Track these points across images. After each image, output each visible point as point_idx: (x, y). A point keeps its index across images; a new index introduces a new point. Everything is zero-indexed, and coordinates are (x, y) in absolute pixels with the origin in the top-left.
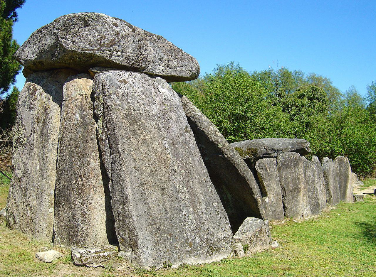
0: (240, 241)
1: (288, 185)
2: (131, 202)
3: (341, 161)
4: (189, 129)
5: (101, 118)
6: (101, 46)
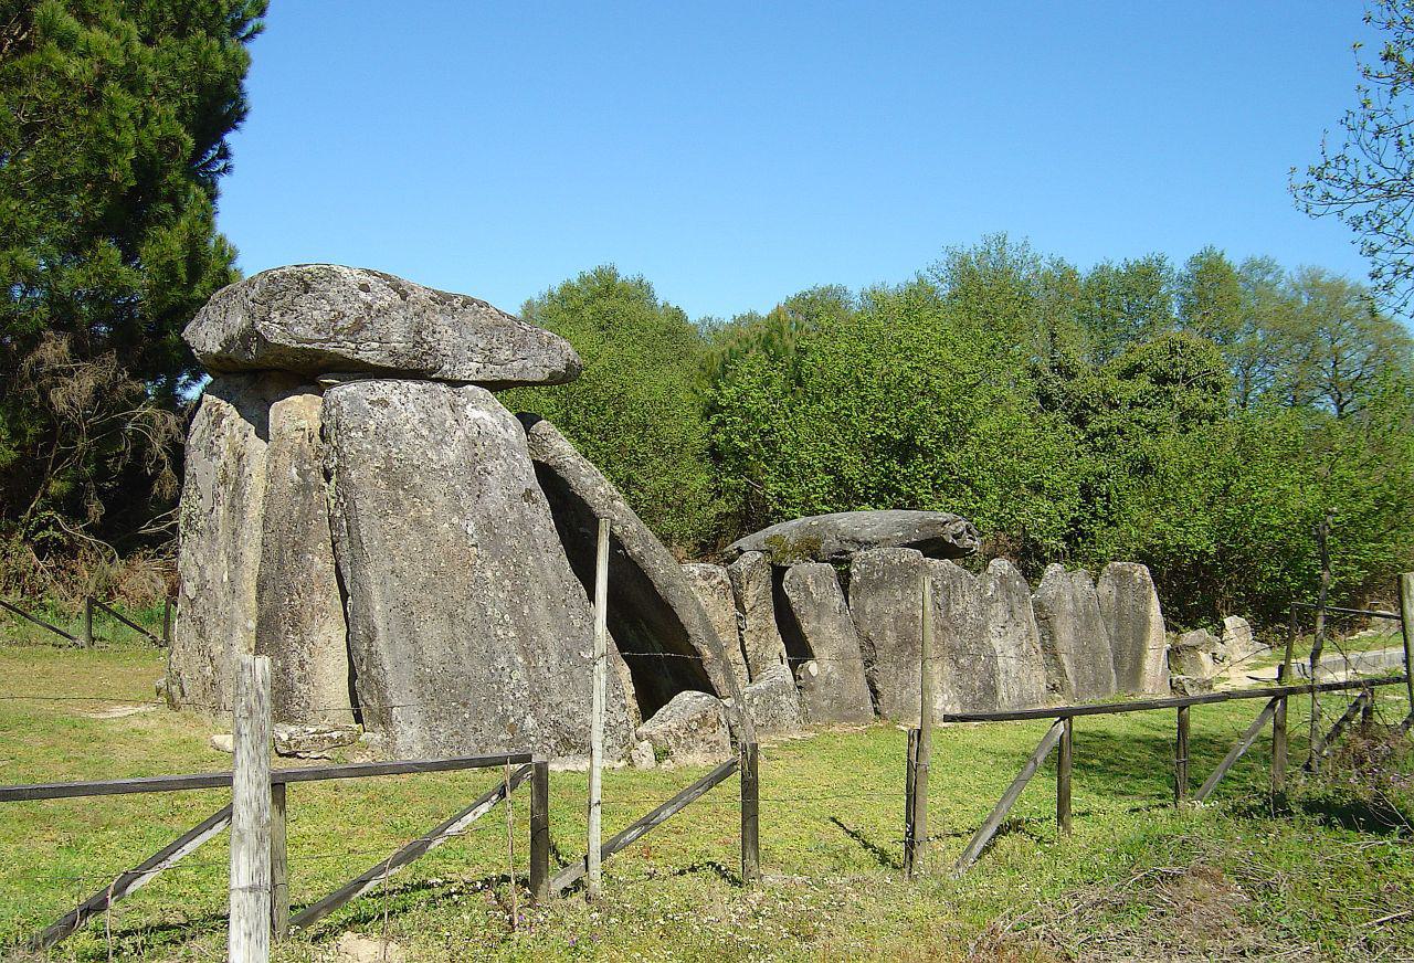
0: (650, 737)
1: (881, 634)
2: (381, 634)
3: (1122, 576)
4: (539, 494)
5: (334, 477)
6: (337, 333)
